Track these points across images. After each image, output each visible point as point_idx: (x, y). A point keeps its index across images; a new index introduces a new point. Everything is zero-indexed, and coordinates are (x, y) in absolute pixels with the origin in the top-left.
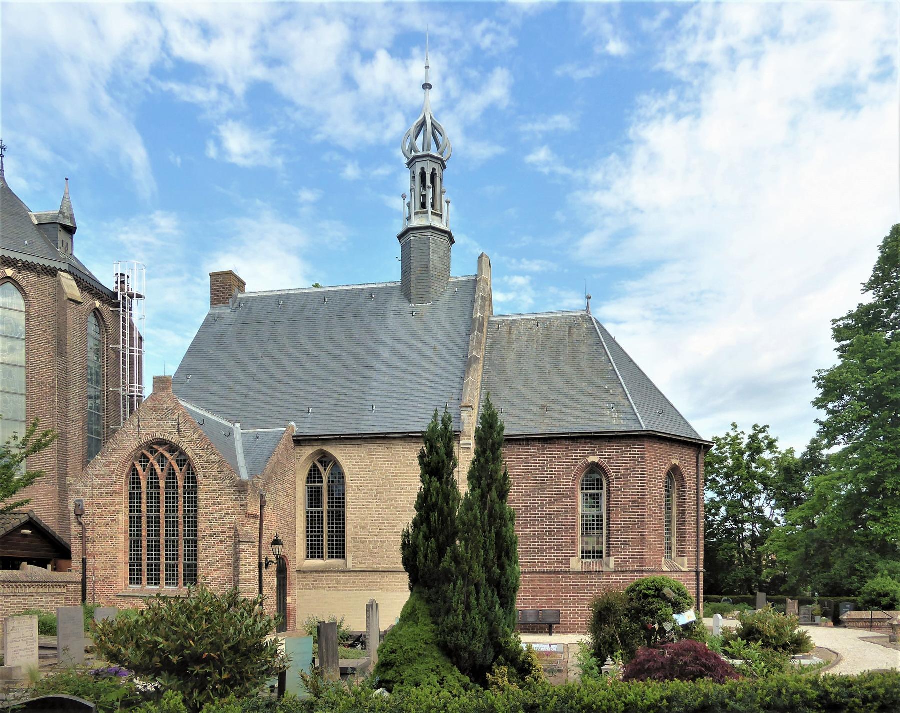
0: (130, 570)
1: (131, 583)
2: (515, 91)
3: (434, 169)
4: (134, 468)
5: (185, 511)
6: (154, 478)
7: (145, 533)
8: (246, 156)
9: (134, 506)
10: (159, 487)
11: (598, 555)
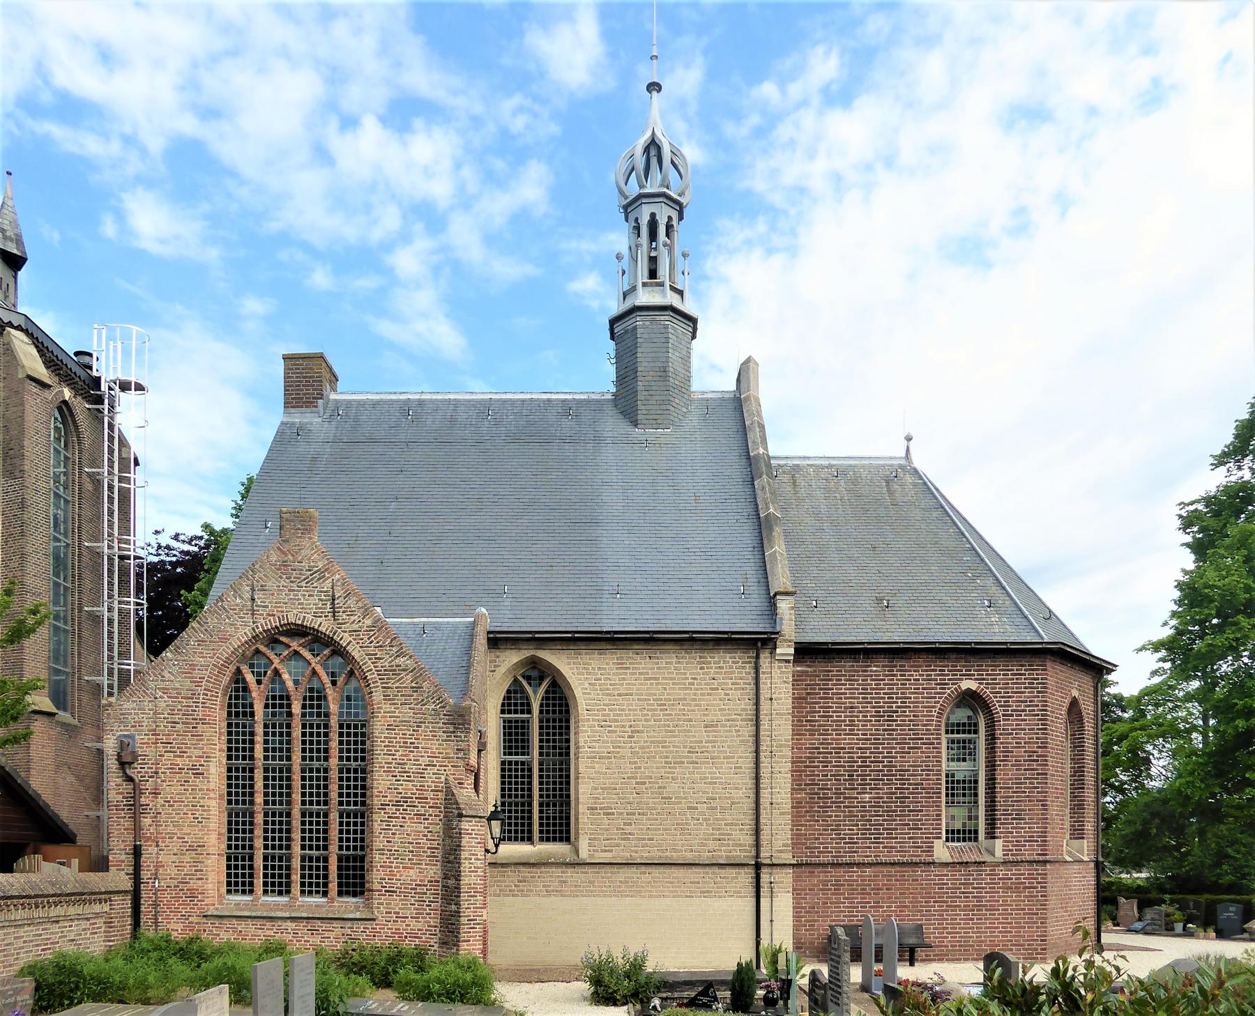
0: (229, 867)
1: (229, 892)
2: (558, 194)
4: (238, 677)
5: (341, 758)
6: (279, 701)
7: (259, 799)
8: (162, 241)
9: (239, 746)
11: (968, 835)
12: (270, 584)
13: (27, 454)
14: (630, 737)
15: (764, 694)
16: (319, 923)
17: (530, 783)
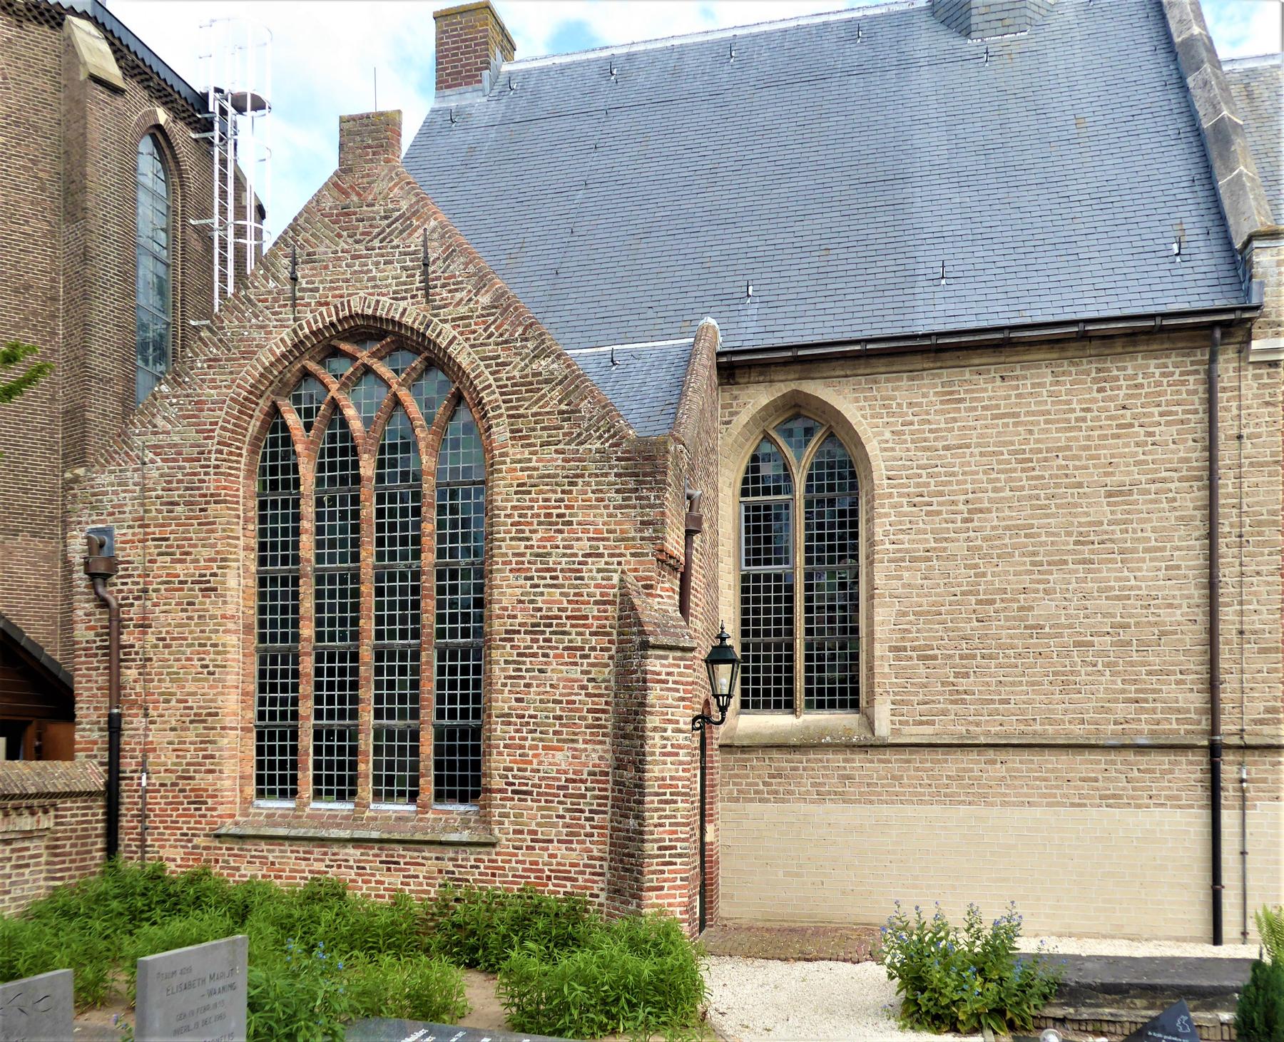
0: (260, 751)
1: (260, 794)
5: (441, 553)
6: (338, 454)
9: (275, 546)
10: (357, 479)
12: (322, 249)
13: (90, 184)
14: (966, 521)
15: (1226, 426)
16: (400, 850)
17: (790, 610)
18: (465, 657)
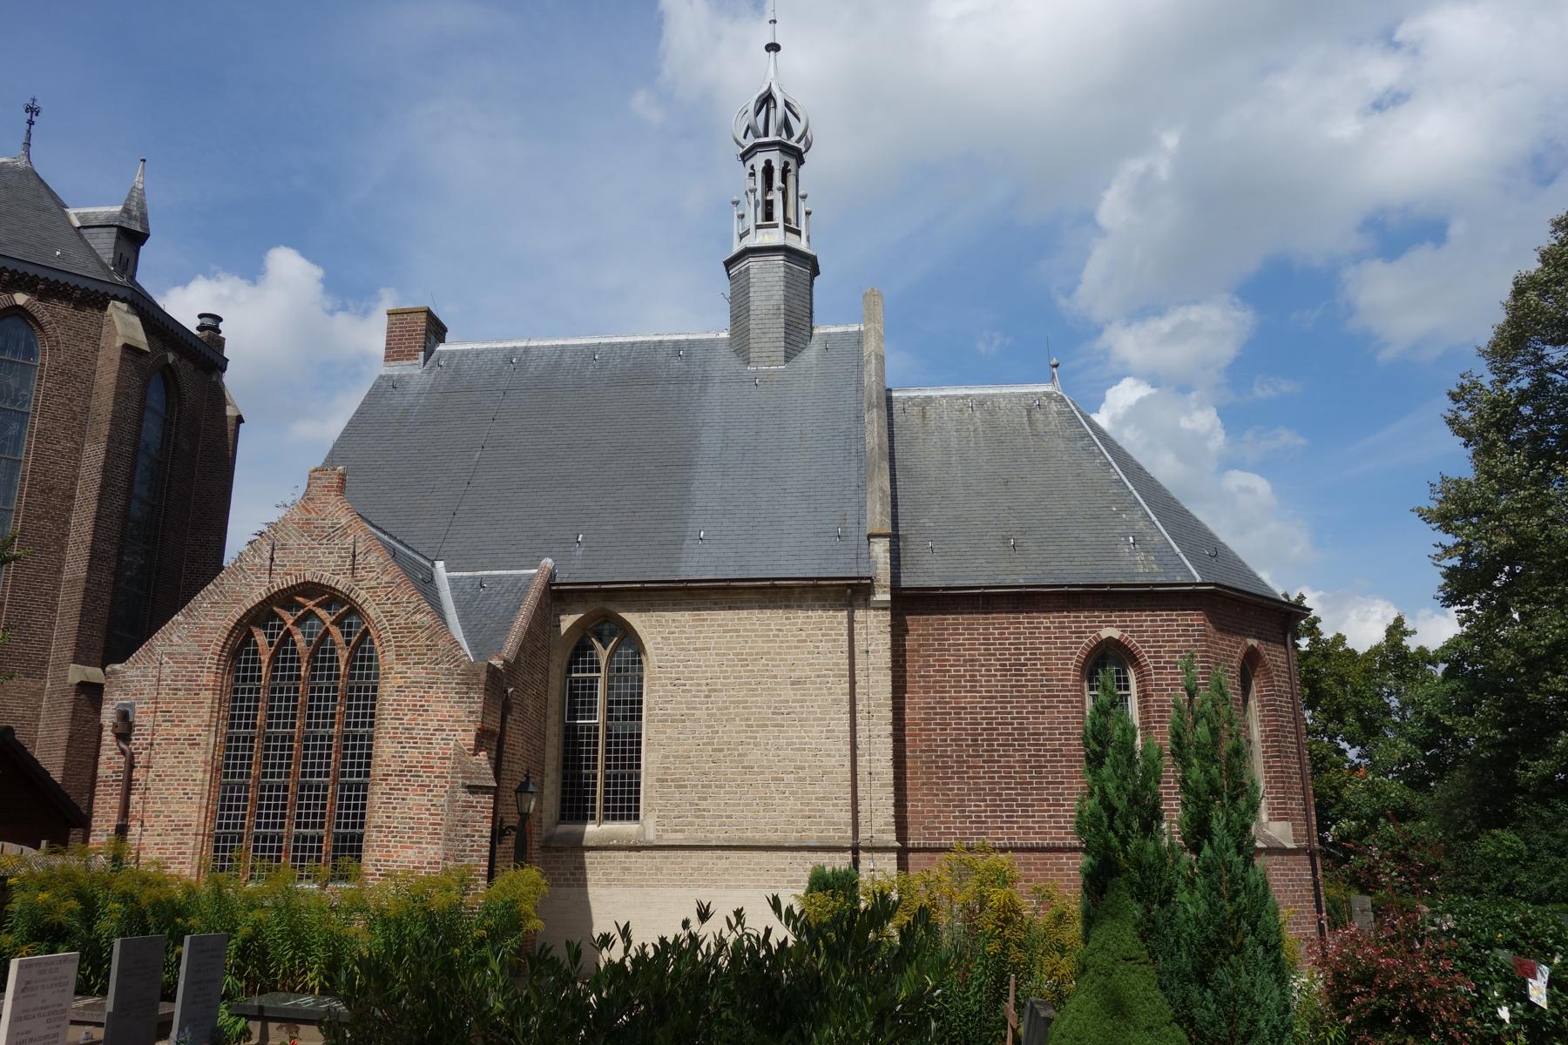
3: (787, 164)
15: (860, 646)
18: (272, 841)
